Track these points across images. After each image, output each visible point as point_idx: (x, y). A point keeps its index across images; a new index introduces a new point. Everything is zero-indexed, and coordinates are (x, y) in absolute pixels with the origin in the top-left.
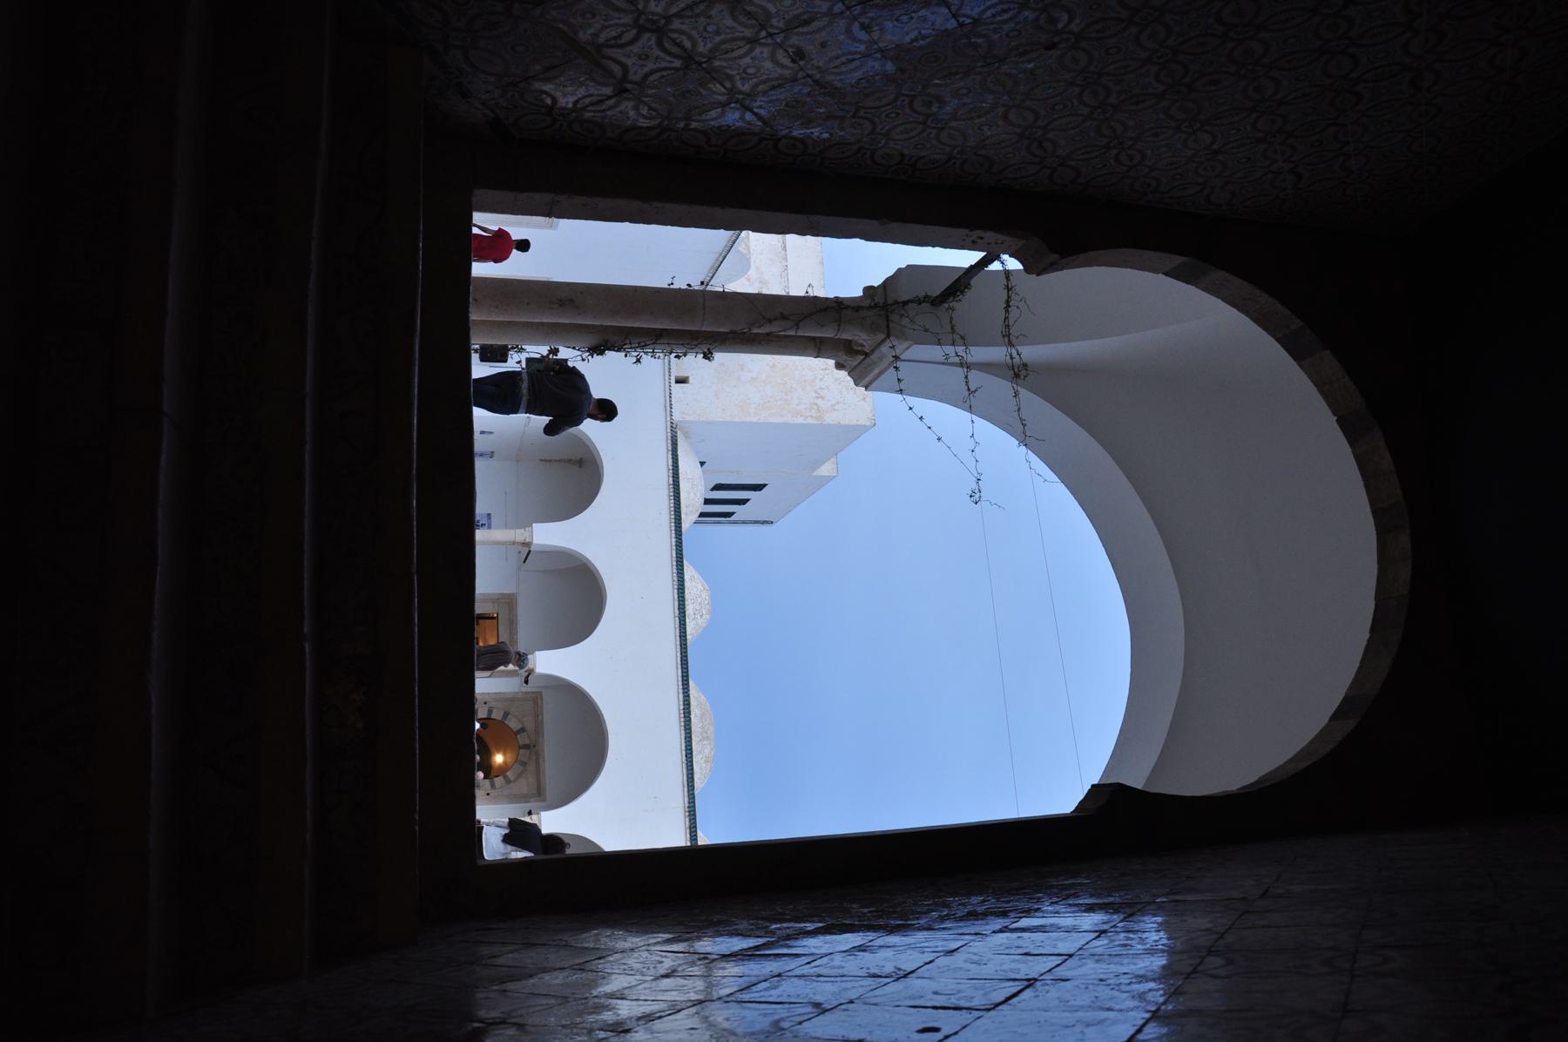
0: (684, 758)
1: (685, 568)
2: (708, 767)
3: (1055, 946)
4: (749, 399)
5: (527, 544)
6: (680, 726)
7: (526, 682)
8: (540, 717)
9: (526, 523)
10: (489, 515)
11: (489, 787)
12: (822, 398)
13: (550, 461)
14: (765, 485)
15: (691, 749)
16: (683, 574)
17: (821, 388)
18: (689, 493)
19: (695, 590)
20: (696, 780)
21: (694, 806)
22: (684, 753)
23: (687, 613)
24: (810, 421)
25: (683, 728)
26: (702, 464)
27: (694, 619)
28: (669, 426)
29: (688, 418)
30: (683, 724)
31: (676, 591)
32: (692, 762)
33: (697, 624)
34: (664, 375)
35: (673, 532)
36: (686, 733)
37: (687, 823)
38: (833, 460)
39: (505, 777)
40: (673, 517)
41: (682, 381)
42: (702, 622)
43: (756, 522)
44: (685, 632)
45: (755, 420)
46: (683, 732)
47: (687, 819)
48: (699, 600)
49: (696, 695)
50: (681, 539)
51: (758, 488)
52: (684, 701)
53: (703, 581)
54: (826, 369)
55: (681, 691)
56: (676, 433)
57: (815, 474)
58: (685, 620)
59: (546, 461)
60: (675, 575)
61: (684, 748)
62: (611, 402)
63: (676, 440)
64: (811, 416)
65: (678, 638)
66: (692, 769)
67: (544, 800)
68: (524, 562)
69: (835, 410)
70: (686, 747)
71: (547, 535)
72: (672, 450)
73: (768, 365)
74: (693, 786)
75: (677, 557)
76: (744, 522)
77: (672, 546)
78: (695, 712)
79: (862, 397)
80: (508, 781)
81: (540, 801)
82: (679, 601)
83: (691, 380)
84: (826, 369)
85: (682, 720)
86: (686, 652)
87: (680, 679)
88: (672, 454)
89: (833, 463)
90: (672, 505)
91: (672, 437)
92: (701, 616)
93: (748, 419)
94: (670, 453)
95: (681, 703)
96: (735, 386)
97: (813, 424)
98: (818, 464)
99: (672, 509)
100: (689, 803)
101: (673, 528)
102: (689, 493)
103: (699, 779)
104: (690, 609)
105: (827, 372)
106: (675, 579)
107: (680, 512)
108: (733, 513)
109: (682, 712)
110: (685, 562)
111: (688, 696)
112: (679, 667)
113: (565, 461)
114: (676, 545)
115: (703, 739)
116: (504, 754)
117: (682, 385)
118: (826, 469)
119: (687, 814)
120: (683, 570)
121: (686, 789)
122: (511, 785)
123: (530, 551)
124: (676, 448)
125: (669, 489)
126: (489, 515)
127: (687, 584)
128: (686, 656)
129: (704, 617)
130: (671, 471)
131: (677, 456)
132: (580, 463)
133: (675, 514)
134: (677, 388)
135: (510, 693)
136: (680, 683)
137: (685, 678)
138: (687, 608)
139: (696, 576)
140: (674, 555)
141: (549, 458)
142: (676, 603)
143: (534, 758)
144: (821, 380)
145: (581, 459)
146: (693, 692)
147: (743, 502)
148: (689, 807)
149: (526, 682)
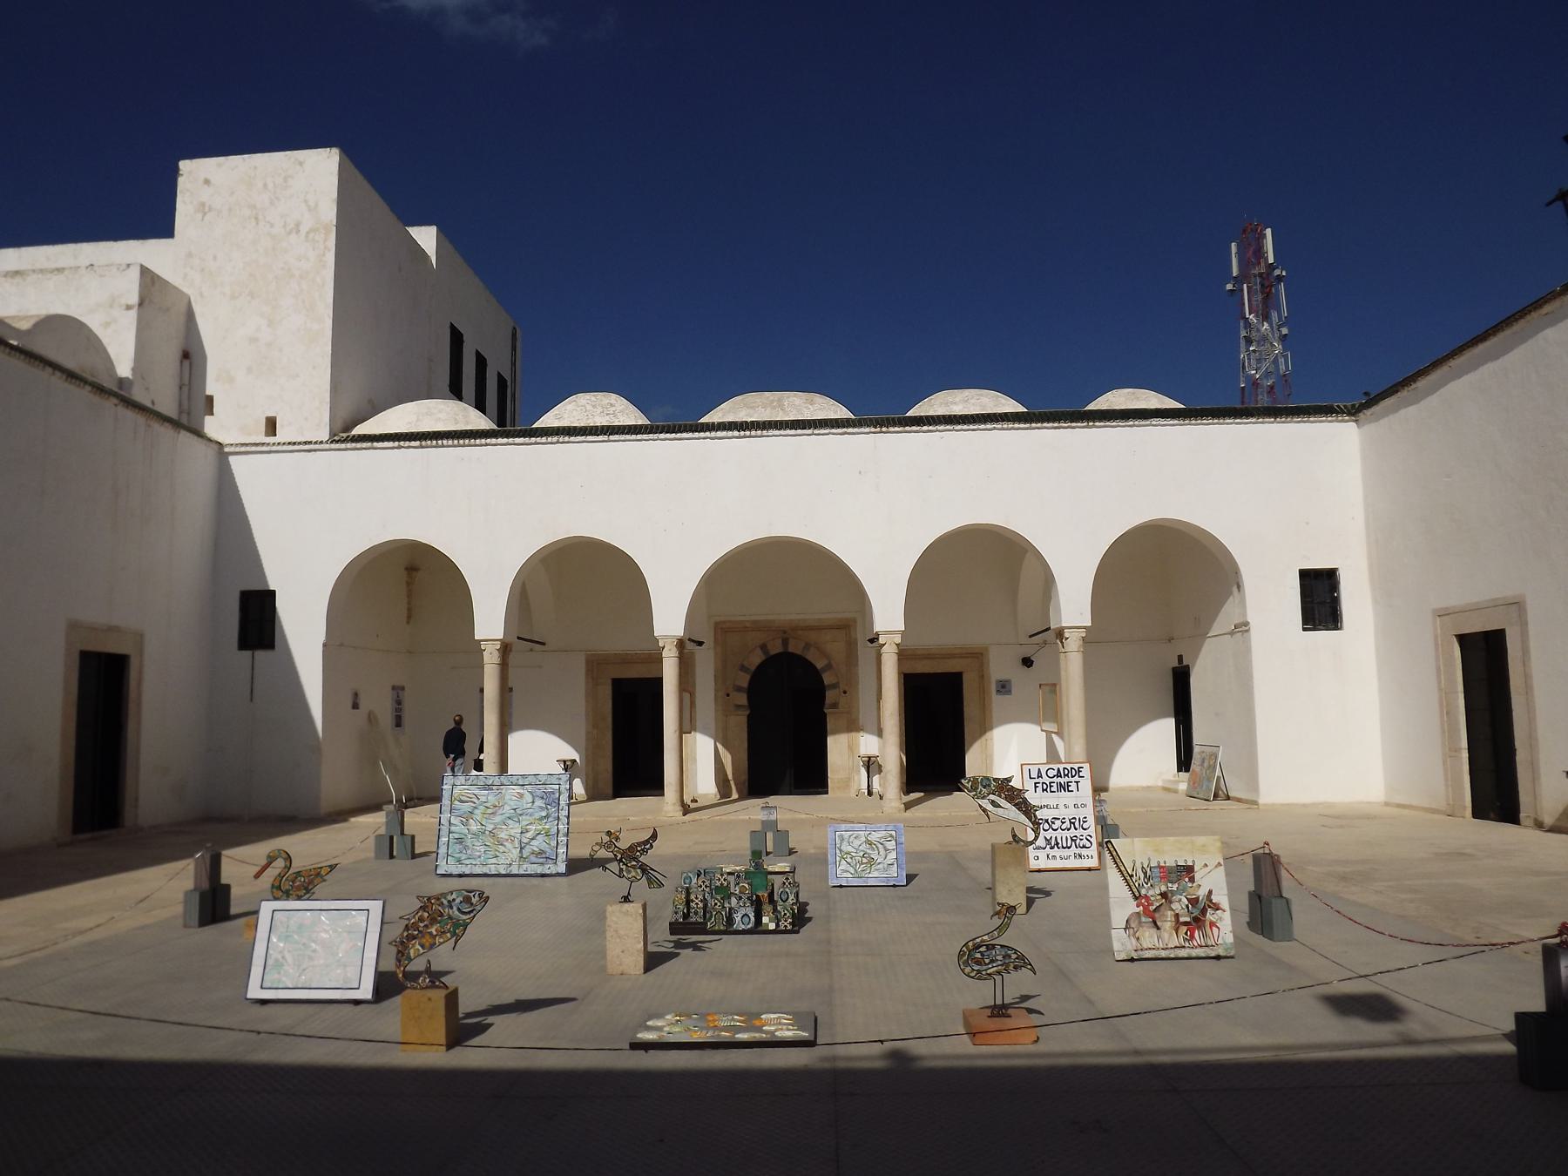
3: (752, 1018)
7: (700, 644)
8: (748, 625)
11: (837, 691)
12: (298, 225)
13: (409, 610)
14: (453, 328)
17: (284, 226)
18: (439, 419)
41: (271, 426)
48: (589, 407)
49: (720, 415)
51: (457, 338)
54: (256, 218)
64: (325, 240)
69: (317, 205)
79: (298, 167)
83: (271, 414)
84: (256, 218)
92: (612, 405)
102: (439, 419)
104: (600, 421)
105: (260, 217)
122: (833, 662)
129: (613, 402)
132: (411, 569)
134: (283, 435)
143: (800, 632)
145: (406, 569)
147: (481, 362)
149: (700, 644)
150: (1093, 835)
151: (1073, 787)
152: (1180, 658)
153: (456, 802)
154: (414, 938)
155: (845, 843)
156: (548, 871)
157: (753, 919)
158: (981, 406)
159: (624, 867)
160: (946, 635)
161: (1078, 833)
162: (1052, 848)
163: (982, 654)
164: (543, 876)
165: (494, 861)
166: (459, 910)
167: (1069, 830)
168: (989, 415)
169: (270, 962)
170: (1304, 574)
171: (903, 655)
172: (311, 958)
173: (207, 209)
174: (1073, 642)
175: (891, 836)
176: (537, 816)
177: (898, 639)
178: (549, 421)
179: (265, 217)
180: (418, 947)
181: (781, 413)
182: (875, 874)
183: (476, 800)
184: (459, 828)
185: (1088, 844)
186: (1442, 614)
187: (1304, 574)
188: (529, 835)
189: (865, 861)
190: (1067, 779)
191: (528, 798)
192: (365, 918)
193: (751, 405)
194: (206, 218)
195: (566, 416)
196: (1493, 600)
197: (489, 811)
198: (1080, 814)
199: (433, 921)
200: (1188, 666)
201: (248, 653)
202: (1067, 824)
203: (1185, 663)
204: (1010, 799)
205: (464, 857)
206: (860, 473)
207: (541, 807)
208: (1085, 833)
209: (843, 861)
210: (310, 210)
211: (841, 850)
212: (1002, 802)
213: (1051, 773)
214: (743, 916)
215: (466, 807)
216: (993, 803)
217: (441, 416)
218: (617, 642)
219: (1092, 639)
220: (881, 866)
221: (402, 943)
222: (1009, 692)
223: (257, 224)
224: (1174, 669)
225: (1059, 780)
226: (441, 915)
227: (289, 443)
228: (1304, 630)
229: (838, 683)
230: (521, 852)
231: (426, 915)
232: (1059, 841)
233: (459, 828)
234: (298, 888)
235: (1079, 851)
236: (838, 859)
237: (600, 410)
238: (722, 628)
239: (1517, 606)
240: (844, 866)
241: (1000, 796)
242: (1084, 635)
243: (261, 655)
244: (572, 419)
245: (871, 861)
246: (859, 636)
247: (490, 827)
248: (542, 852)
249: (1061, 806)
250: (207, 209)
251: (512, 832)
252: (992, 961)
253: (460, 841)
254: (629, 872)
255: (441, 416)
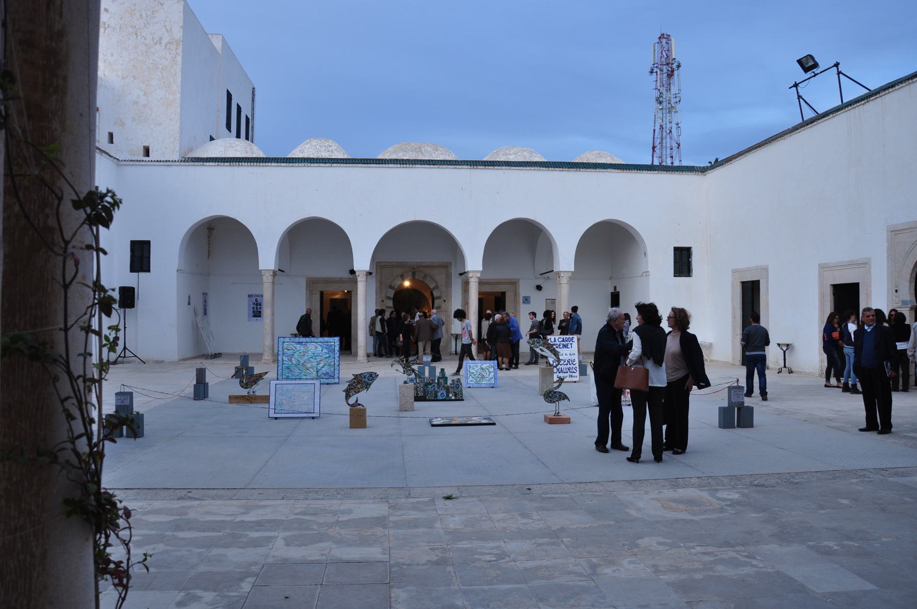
0: (436, 166)
1: (294, 157)
2: (441, 149)
4: (161, 99)
5: (274, 274)
6: (412, 167)
8: (394, 264)
9: (259, 274)
10: (249, 296)
12: (161, 39)
13: (209, 251)
14: (228, 91)
15: (429, 161)
16: (299, 158)
17: (153, 39)
20: (450, 159)
21: (470, 161)
22: (432, 166)
24: (180, 51)
25: (414, 166)
26: (212, 139)
28: (184, 164)
29: (178, 149)
30: (411, 166)
31: (312, 165)
32: (438, 161)
33: (335, 150)
34: (142, 165)
35: (267, 164)
36: (418, 164)
37: (481, 167)
38: (210, 36)
39: (434, 289)
40: (255, 164)
41: (147, 152)
42: (334, 146)
43: (253, 100)
44: (343, 159)
45: (179, 95)
46: (417, 166)
47: (479, 167)
48: (318, 147)
50: (272, 158)
51: (229, 96)
52: (394, 163)
53: (303, 144)
54: (136, 34)
55: (387, 165)
56: (189, 158)
57: (220, 52)
58: (334, 159)
59: (209, 255)
60: (300, 165)
61: (428, 166)
62: (770, 342)
63: (195, 158)
64: (176, 49)
65: (347, 165)
66: (443, 161)
67: (451, 263)
68: (283, 271)
70: (427, 164)
71: (267, 259)
72: (203, 162)
74: (455, 161)
75: (286, 163)
76: (253, 109)
77: (277, 166)
78: (401, 156)
79: (160, 6)
80: (437, 287)
81: (451, 264)
82: (320, 163)
83: (146, 144)
84: (136, 34)
85: (408, 166)
86: (358, 160)
87: (378, 165)
88: (206, 162)
89: (180, 38)
90: (246, 164)
91: (193, 162)
92: (330, 146)
93: (178, 101)
94: (205, 163)
95: (396, 166)
96: (151, 109)
97: (183, 47)
98: (213, 49)
99: (249, 164)
100: (468, 165)
101: (264, 164)
103: (449, 156)
105: (139, 33)
106: (303, 164)
107: (252, 158)
108: (247, 116)
109: (402, 166)
110: (289, 156)
111: (390, 160)
112: (369, 165)
113: (209, 241)
114: (277, 162)
115: (421, 151)
116: (401, 285)
117: (150, 151)
118: (217, 43)
119: (475, 167)
120: (296, 158)
121: (458, 167)
122: (438, 285)
123: (279, 270)
124: (201, 158)
125: (233, 166)
126: (249, 296)
127: (306, 155)
128: (361, 160)
129: (331, 144)
130: (220, 163)
131: (207, 158)
133: (253, 162)
135: (376, 284)
136: (381, 165)
137: (375, 162)
138: (324, 157)
139: (299, 148)
140: (285, 164)
141: (207, 253)
142: (322, 165)
146: (387, 156)
148: (471, 166)
150: (578, 367)
151: (569, 346)
152: (615, 288)
153: (285, 350)
154: (352, 389)
155: (471, 369)
156: (331, 382)
157: (445, 395)
158: (523, 156)
159: (405, 370)
160: (501, 274)
161: (571, 366)
162: (560, 373)
163: (516, 283)
164: (328, 384)
165: (305, 377)
166: (368, 379)
167: (567, 365)
168: (527, 162)
169: (277, 403)
170: (676, 249)
171: (481, 283)
172: (294, 402)
173: (106, 26)
174: (564, 280)
175: (492, 366)
176: (324, 356)
177: (479, 275)
178: (297, 154)
179: (141, 34)
180: (353, 392)
181: (421, 155)
182: (485, 382)
183: (294, 349)
184: (287, 363)
185: (575, 371)
186: (735, 272)
187: (676, 249)
188: (321, 365)
189: (480, 376)
190: (567, 343)
191: (320, 348)
192: (313, 387)
193: (405, 150)
194: (106, 31)
195: (305, 151)
196: (756, 267)
197: (301, 354)
198: (572, 357)
199: (359, 383)
200: (619, 292)
201: (136, 274)
202: (566, 363)
203: (617, 291)
204: (548, 348)
205: (290, 375)
206: (462, 189)
207: (326, 353)
208: (574, 366)
209: (471, 377)
210: (167, 31)
211: (469, 372)
212: (545, 349)
213: (560, 340)
214: (441, 393)
215: (290, 352)
216: (541, 350)
217: (238, 148)
218: (332, 271)
219: (574, 276)
220: (487, 379)
221: (347, 391)
222: (529, 303)
223: (137, 37)
224: (612, 293)
225: (564, 343)
226: (362, 381)
227: (157, 161)
228: (675, 276)
229: (441, 296)
230: (317, 373)
231: (356, 381)
232: (563, 369)
233: (287, 363)
234: (252, 382)
235: (571, 374)
236: (468, 376)
237: (324, 149)
238: (380, 266)
239: (765, 270)
240: (471, 378)
241: (544, 347)
242: (570, 275)
243: (142, 274)
244: (309, 153)
245: (483, 377)
246: (452, 272)
247: (302, 362)
248: (327, 373)
249: (564, 354)
250: (106, 26)
251: (313, 364)
252: (555, 397)
253: (288, 368)
254: (407, 372)
255: (238, 148)
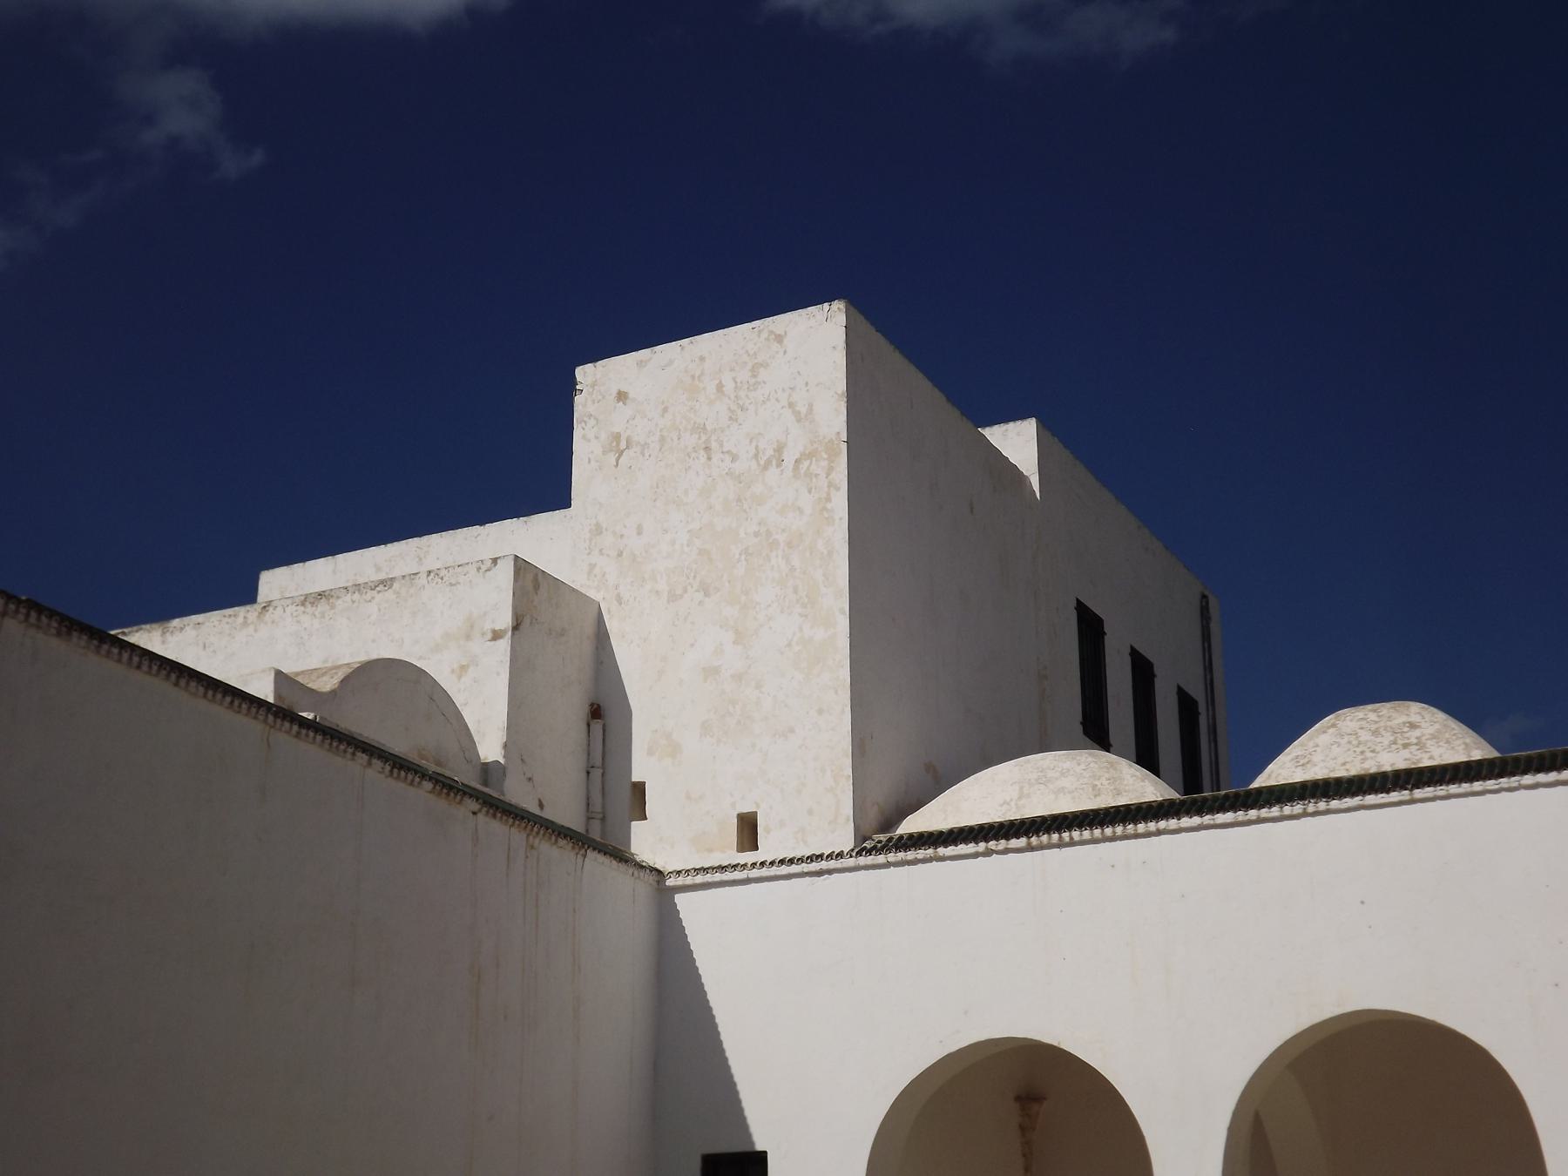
12: (779, 449)
14: (1081, 608)
17: (756, 456)
18: (1062, 790)
19: (1336, 750)
23: (1402, 765)
27: (1420, 745)
48: (1365, 736)
54: (707, 449)
73: (701, 603)
79: (775, 346)
84: (707, 449)
92: (1413, 726)
96: (758, 686)
104: (1391, 760)
105: (714, 445)
129: (1415, 718)
134: (769, 848)
144: (734, 458)
145: (1018, 1098)
147: (1142, 670)
